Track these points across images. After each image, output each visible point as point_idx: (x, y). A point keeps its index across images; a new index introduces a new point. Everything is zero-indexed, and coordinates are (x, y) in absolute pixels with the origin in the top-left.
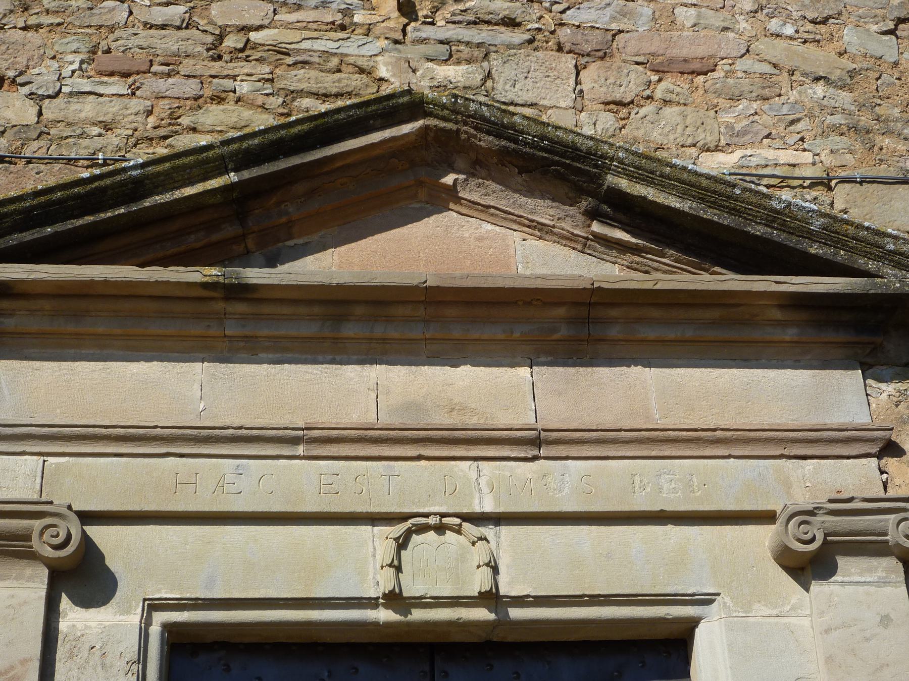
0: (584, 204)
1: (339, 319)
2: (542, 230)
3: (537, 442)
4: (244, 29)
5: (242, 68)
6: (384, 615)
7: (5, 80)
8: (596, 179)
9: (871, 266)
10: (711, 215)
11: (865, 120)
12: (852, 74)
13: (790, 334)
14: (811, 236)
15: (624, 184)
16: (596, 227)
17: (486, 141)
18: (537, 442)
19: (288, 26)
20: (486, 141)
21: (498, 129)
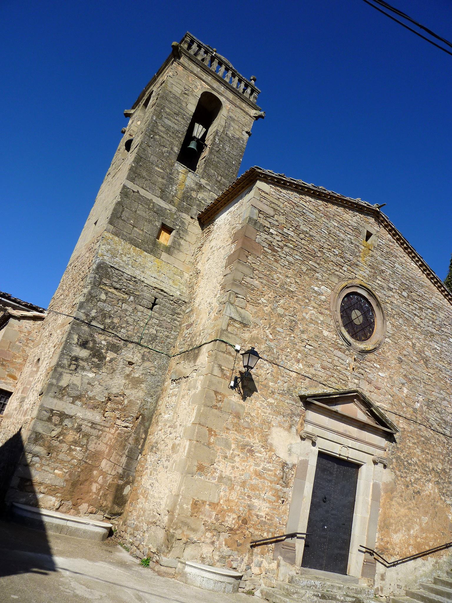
0: (367, 409)
1: (342, 417)
2: (361, 410)
3: (356, 440)
4: (337, 366)
5: (336, 373)
6: (338, 456)
7: (203, 127)
8: (370, 407)
9: (392, 429)
10: (380, 417)
11: (393, 403)
12: (393, 395)
13: (381, 433)
14: (388, 423)
15: (373, 410)
16: (367, 412)
17: (362, 398)
18: (356, 440)
19: (341, 367)
20: (362, 398)
21: (364, 398)
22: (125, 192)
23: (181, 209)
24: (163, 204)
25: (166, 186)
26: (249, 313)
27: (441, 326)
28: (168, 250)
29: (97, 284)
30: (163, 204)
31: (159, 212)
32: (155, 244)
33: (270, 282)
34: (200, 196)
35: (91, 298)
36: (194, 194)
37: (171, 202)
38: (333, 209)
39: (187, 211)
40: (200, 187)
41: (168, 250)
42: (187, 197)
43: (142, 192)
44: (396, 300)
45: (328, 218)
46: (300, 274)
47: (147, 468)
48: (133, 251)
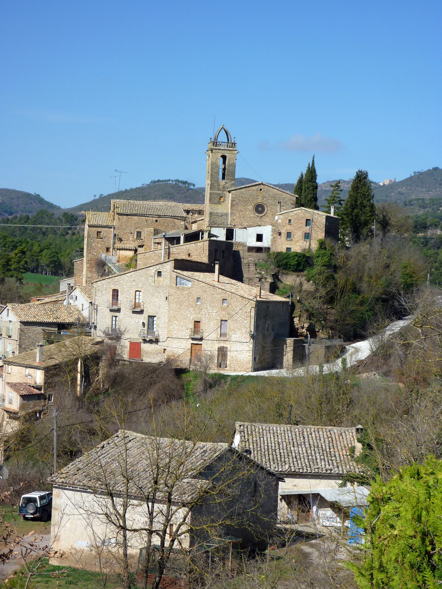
22: (210, 194)
23: (223, 191)
24: (219, 192)
25: (218, 187)
26: (235, 218)
27: (286, 202)
28: (223, 202)
29: (210, 216)
30: (219, 192)
31: (219, 194)
32: (220, 202)
33: (238, 210)
34: (227, 185)
35: (210, 219)
36: (225, 186)
37: (221, 191)
38: (249, 188)
39: (225, 191)
40: (226, 183)
41: (223, 202)
42: (224, 187)
43: (214, 192)
44: (270, 201)
45: (249, 191)
46: (244, 206)
47: (413, 314)
48: (215, 206)
